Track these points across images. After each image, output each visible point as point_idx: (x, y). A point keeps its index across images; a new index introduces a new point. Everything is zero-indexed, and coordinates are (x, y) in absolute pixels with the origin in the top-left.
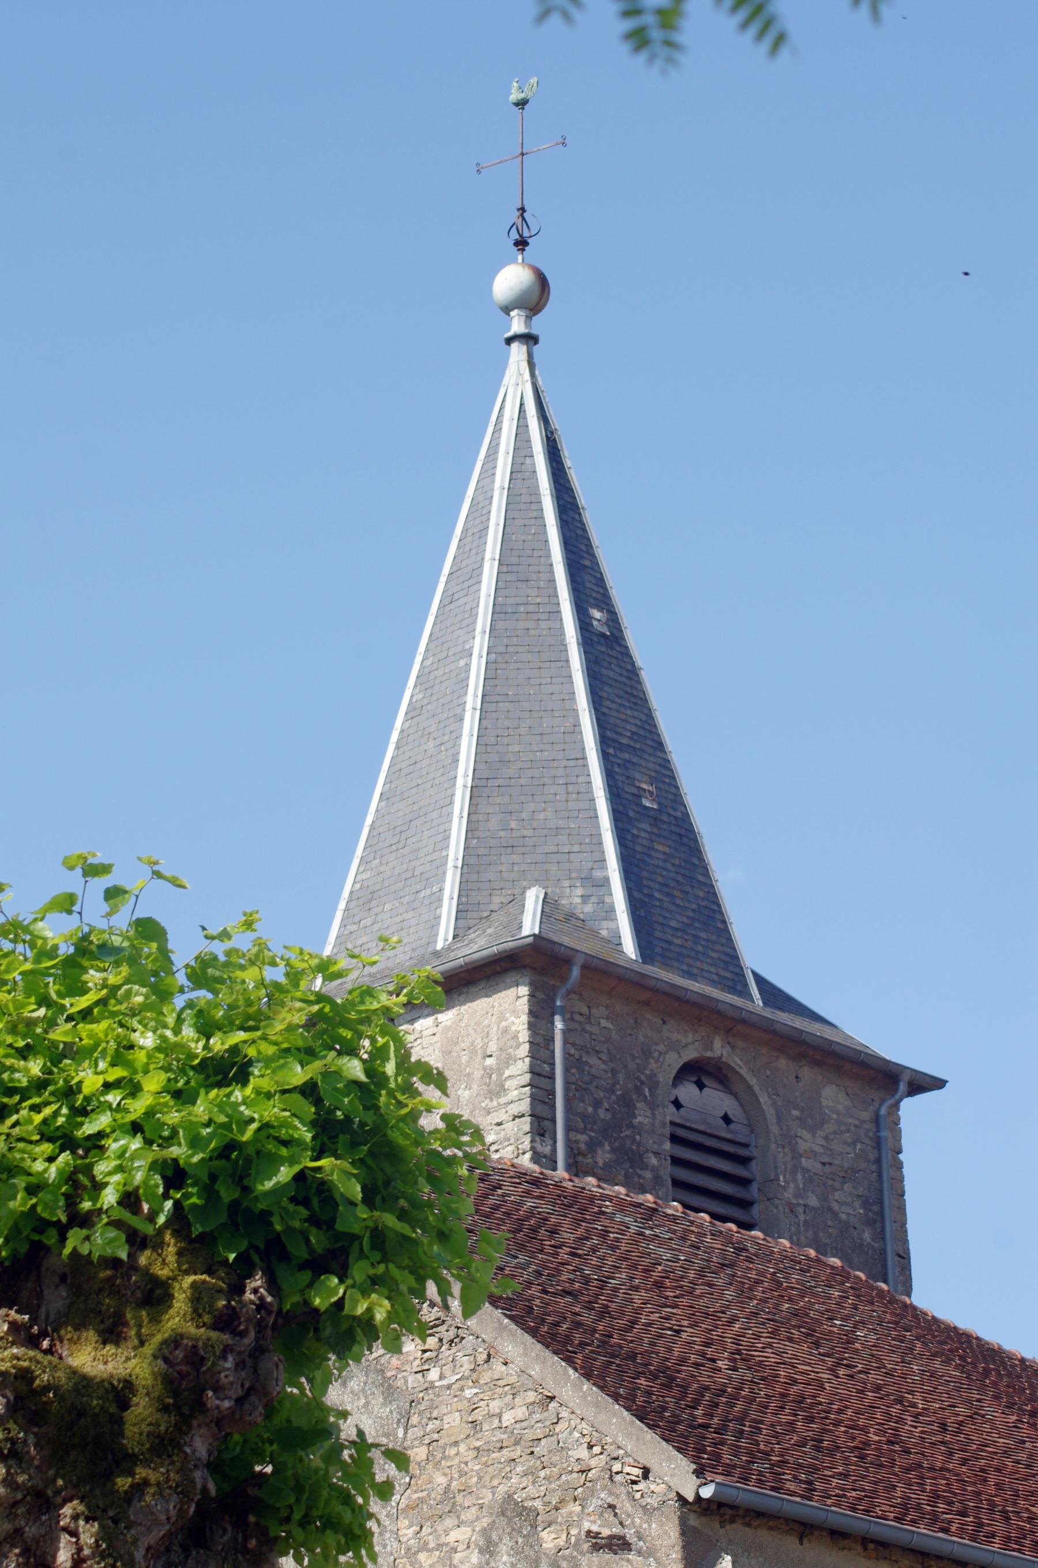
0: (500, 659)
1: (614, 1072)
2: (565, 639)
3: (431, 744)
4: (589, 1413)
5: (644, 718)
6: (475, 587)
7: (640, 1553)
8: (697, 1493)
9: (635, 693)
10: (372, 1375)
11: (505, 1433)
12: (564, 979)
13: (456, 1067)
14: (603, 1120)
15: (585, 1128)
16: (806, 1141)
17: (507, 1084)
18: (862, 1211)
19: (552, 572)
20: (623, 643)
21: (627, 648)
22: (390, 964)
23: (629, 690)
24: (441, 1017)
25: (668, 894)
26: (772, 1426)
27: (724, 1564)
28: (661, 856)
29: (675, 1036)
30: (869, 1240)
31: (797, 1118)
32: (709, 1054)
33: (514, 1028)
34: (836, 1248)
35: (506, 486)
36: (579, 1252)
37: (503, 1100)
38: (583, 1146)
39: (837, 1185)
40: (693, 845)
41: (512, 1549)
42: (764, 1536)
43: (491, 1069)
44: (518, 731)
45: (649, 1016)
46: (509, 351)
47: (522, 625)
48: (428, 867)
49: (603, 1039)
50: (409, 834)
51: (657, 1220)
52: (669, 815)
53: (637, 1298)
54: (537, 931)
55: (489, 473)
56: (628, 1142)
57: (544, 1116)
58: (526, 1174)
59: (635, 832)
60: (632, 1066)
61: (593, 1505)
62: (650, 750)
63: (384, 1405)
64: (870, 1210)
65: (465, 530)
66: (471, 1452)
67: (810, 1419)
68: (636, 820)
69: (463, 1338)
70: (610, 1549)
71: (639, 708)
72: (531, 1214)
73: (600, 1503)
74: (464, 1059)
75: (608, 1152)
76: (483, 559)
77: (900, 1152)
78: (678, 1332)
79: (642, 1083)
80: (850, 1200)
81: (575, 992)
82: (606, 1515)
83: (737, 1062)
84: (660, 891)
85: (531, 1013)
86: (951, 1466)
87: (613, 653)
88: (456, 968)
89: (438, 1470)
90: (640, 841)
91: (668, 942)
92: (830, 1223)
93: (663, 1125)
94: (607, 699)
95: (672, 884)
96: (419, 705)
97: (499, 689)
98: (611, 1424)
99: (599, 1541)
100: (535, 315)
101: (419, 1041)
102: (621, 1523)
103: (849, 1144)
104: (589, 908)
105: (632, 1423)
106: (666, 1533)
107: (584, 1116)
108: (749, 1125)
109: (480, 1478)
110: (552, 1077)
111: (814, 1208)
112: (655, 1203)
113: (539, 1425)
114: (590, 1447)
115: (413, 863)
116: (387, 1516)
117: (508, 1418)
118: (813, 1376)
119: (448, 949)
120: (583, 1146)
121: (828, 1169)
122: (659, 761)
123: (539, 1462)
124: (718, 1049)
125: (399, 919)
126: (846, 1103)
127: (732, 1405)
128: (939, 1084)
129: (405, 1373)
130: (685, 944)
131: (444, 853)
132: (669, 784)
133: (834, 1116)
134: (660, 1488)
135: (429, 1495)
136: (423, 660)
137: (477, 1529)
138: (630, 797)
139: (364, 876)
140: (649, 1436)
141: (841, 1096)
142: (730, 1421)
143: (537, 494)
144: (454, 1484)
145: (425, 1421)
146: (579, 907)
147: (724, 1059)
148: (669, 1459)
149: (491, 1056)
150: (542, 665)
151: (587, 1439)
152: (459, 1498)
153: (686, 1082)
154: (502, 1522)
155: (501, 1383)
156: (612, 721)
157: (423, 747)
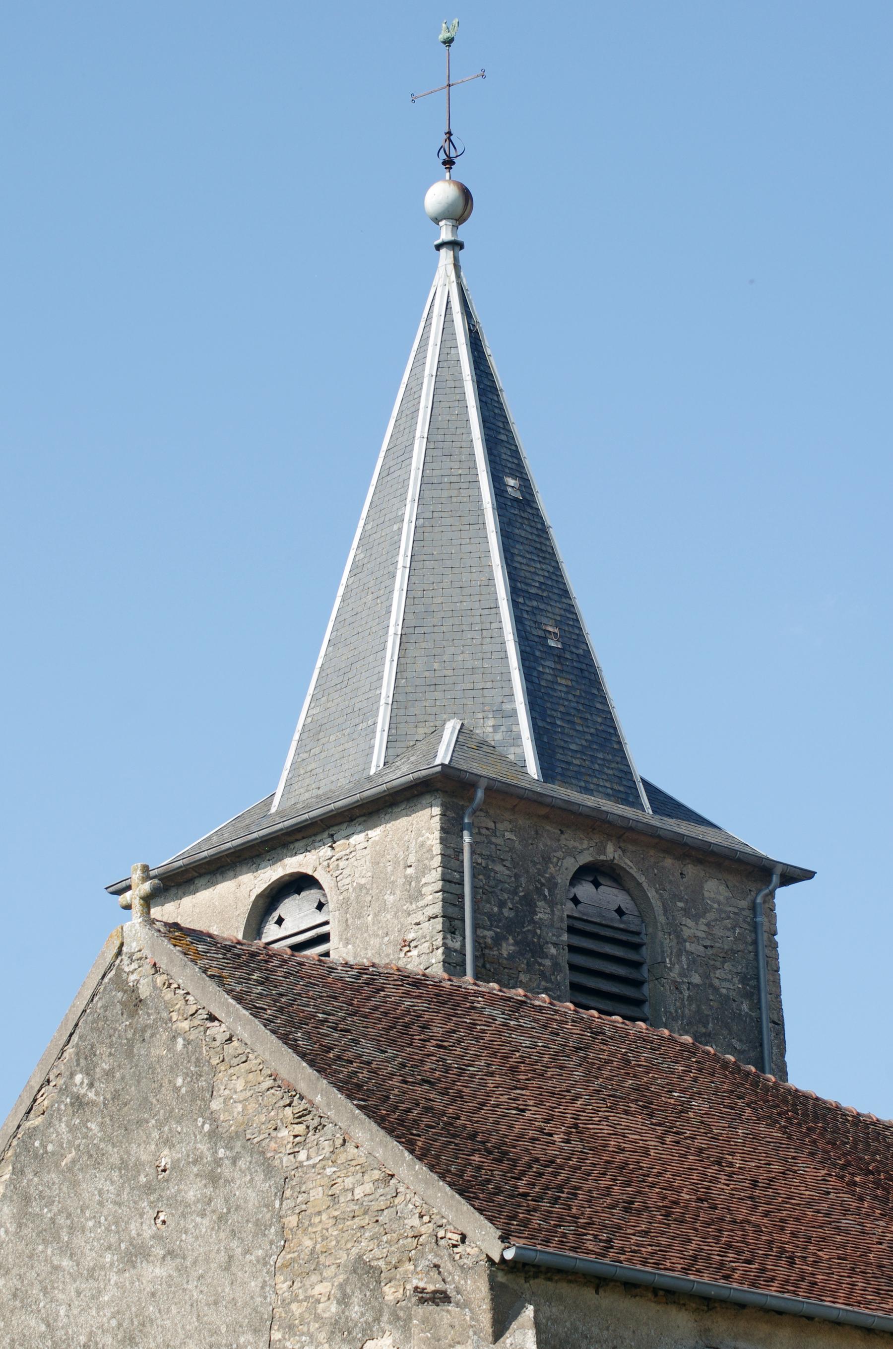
0: (427, 524)
1: (517, 876)
2: (482, 504)
3: (370, 597)
4: (421, 1188)
5: (551, 570)
6: (407, 462)
7: (458, 1305)
8: (502, 1255)
9: (544, 549)
10: (255, 1156)
11: (356, 1204)
12: (471, 799)
13: (382, 875)
14: (507, 918)
15: (492, 925)
16: (690, 928)
17: (424, 890)
18: (740, 986)
19: (472, 447)
20: (534, 505)
21: (538, 509)
22: (333, 787)
23: (538, 546)
24: (371, 833)
25: (569, 722)
26: (590, 1191)
27: (527, 1312)
28: (564, 689)
29: (572, 844)
30: (746, 1010)
31: (682, 909)
32: (602, 857)
33: (429, 842)
34: (717, 1019)
35: (434, 374)
36: (445, 1044)
37: (421, 903)
38: (489, 941)
39: (718, 964)
40: (593, 677)
41: (362, 1300)
42: (564, 1288)
43: (411, 877)
44: (441, 585)
45: (548, 828)
46: (439, 256)
47: (446, 493)
48: (364, 704)
49: (507, 849)
50: (350, 675)
51: (525, 1010)
52: (572, 653)
53: (491, 1083)
54: (447, 762)
55: (421, 362)
56: (530, 936)
57: (454, 916)
58: (409, 977)
59: (541, 669)
60: (533, 870)
61: (423, 1264)
62: (556, 597)
63: (265, 1181)
64: (748, 985)
65: (400, 412)
66: (330, 1220)
67: (628, 1183)
68: (542, 658)
69: (324, 1126)
70: (433, 1302)
71: (547, 561)
72: (408, 1011)
73: (427, 1263)
74: (389, 869)
75: (513, 945)
76: (414, 437)
77: (775, 934)
78: (523, 1111)
79: (543, 885)
80: (730, 977)
81: (481, 810)
82: (432, 1274)
83: (627, 863)
84: (562, 719)
85: (443, 829)
86: (753, 1219)
87: (525, 515)
88: (380, 793)
89: (306, 1235)
90: (545, 676)
91: (567, 763)
92: (711, 997)
93: (562, 920)
94: (518, 555)
95: (573, 712)
96: (360, 564)
97: (427, 550)
98: (437, 1198)
99: (424, 1295)
100: (460, 224)
101: (353, 854)
102: (444, 1280)
103: (729, 930)
104: (499, 736)
105: (453, 1197)
106: (478, 1287)
107: (490, 916)
108: (641, 916)
109: (338, 1242)
110: (461, 883)
111: (697, 985)
112: (525, 996)
113: (383, 1198)
114: (421, 1217)
115: (353, 701)
116: (267, 1273)
117: (359, 1193)
118: (641, 1144)
119: (379, 774)
120: (489, 941)
121: (710, 952)
122: (564, 606)
123: (382, 1229)
124: (611, 852)
125: (340, 748)
126: (726, 894)
127: (555, 1175)
128: (808, 875)
129: (280, 1155)
130: (583, 764)
131: (378, 692)
132: (573, 626)
133: (716, 906)
134: (474, 1251)
135: (299, 1256)
136: (365, 525)
137: (336, 1284)
138: (536, 639)
139: (315, 711)
140: (465, 1208)
141: (722, 888)
142: (548, 1189)
143: (461, 380)
144: (318, 1246)
145: (296, 1194)
146: (491, 735)
147: (616, 862)
148: (481, 1227)
149: (411, 866)
150: (463, 528)
151: (418, 1210)
152: (322, 1259)
153: (583, 882)
154: (354, 1278)
155: (354, 1163)
156: (522, 574)
157: (364, 600)
